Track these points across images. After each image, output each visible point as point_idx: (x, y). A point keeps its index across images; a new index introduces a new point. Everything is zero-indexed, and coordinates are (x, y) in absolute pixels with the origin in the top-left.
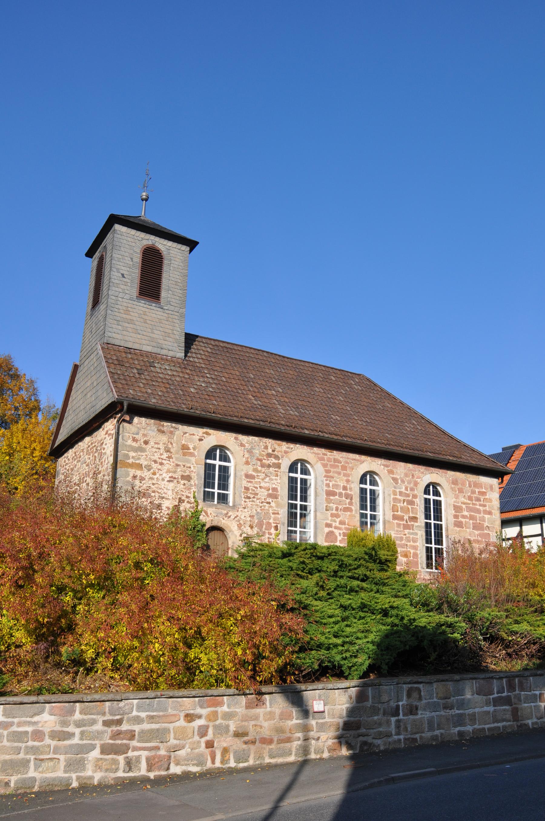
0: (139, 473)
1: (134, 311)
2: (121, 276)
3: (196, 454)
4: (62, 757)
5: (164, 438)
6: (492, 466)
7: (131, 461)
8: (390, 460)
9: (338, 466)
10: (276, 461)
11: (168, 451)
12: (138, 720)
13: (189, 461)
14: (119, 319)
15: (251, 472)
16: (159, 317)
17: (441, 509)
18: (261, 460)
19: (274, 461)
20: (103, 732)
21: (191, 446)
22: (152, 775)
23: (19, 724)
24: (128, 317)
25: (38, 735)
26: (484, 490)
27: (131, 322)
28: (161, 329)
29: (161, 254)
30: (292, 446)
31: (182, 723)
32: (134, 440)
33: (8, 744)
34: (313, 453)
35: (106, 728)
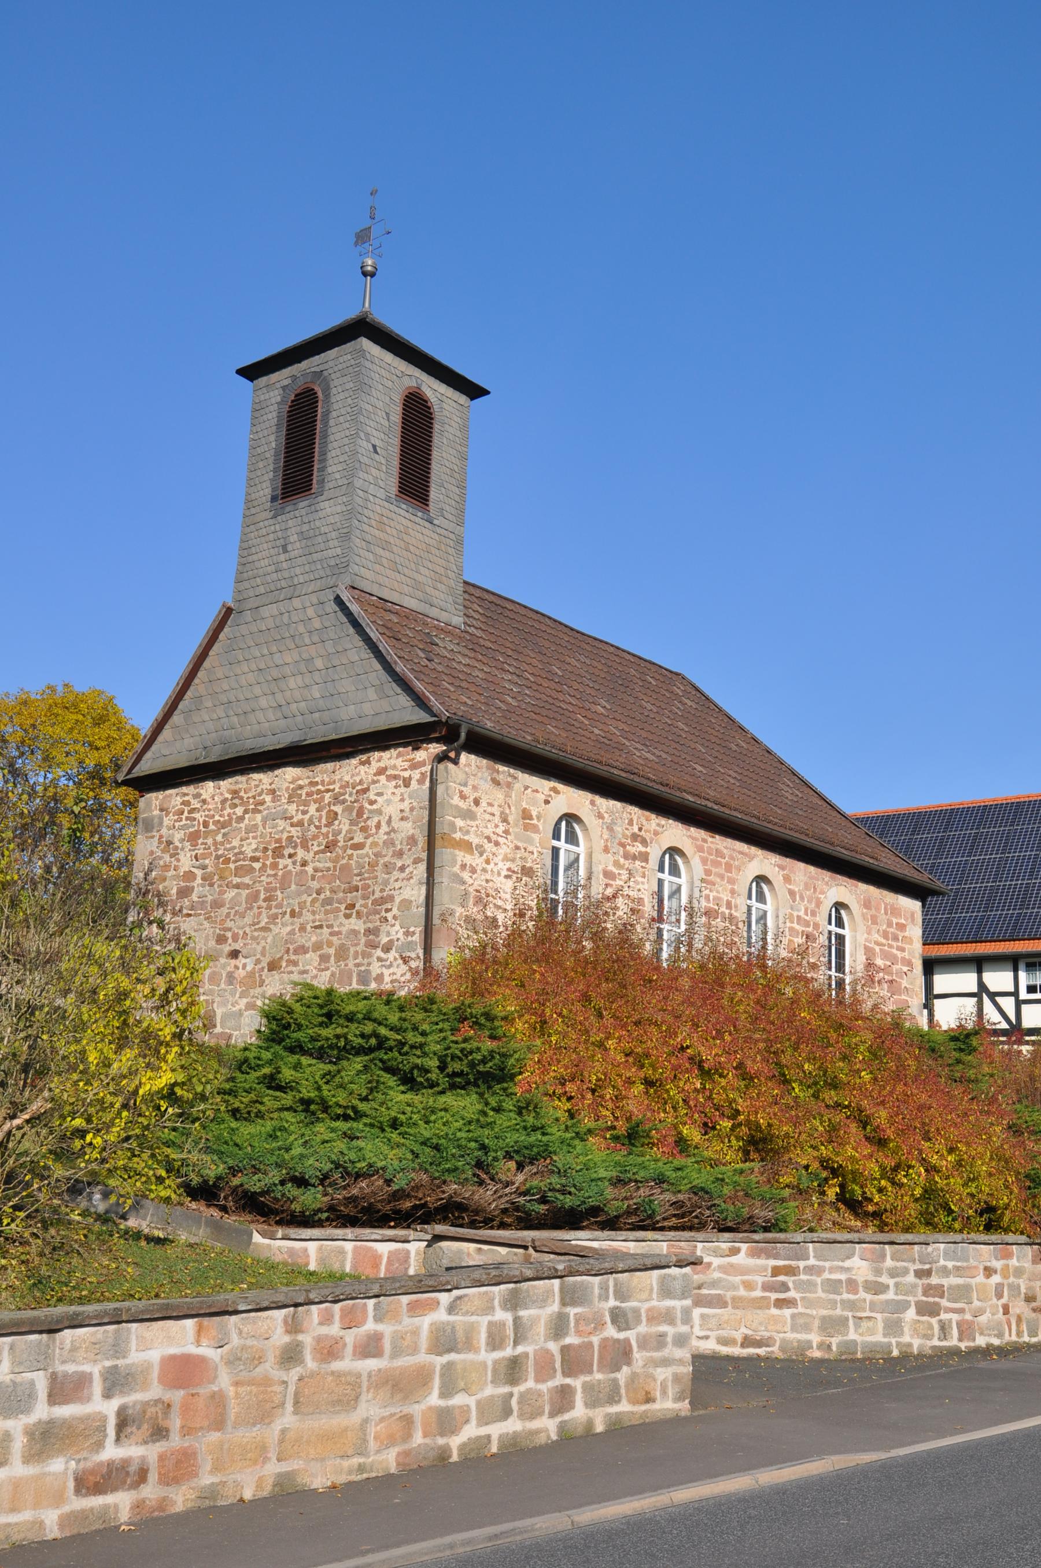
0: (469, 859)
1: (392, 524)
2: (372, 449)
3: (541, 828)
4: (879, 1316)
5: (499, 795)
6: (906, 872)
7: (458, 836)
8: (787, 856)
9: (720, 863)
10: (643, 849)
11: (505, 820)
12: (945, 1272)
13: (531, 841)
14: (368, 538)
15: (611, 868)
16: (427, 540)
17: (844, 951)
18: (623, 845)
19: (642, 848)
20: (915, 1286)
21: (534, 814)
22: (963, 1346)
23: (832, 1270)
24: (381, 535)
25: (852, 1285)
26: (903, 921)
27: (386, 546)
28: (430, 565)
29: (429, 408)
30: (663, 821)
31: (981, 1278)
32: (463, 797)
33: (823, 1295)
34: (690, 836)
35: (918, 1281)
